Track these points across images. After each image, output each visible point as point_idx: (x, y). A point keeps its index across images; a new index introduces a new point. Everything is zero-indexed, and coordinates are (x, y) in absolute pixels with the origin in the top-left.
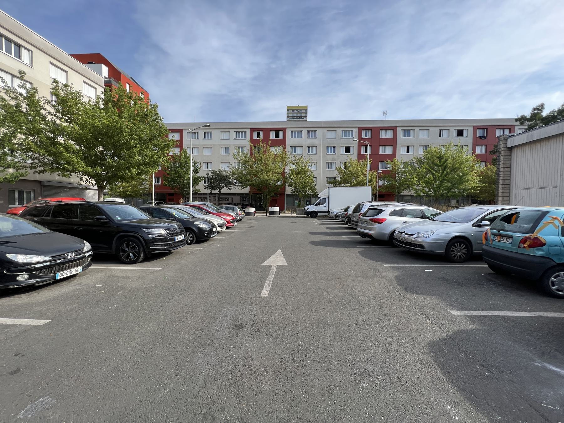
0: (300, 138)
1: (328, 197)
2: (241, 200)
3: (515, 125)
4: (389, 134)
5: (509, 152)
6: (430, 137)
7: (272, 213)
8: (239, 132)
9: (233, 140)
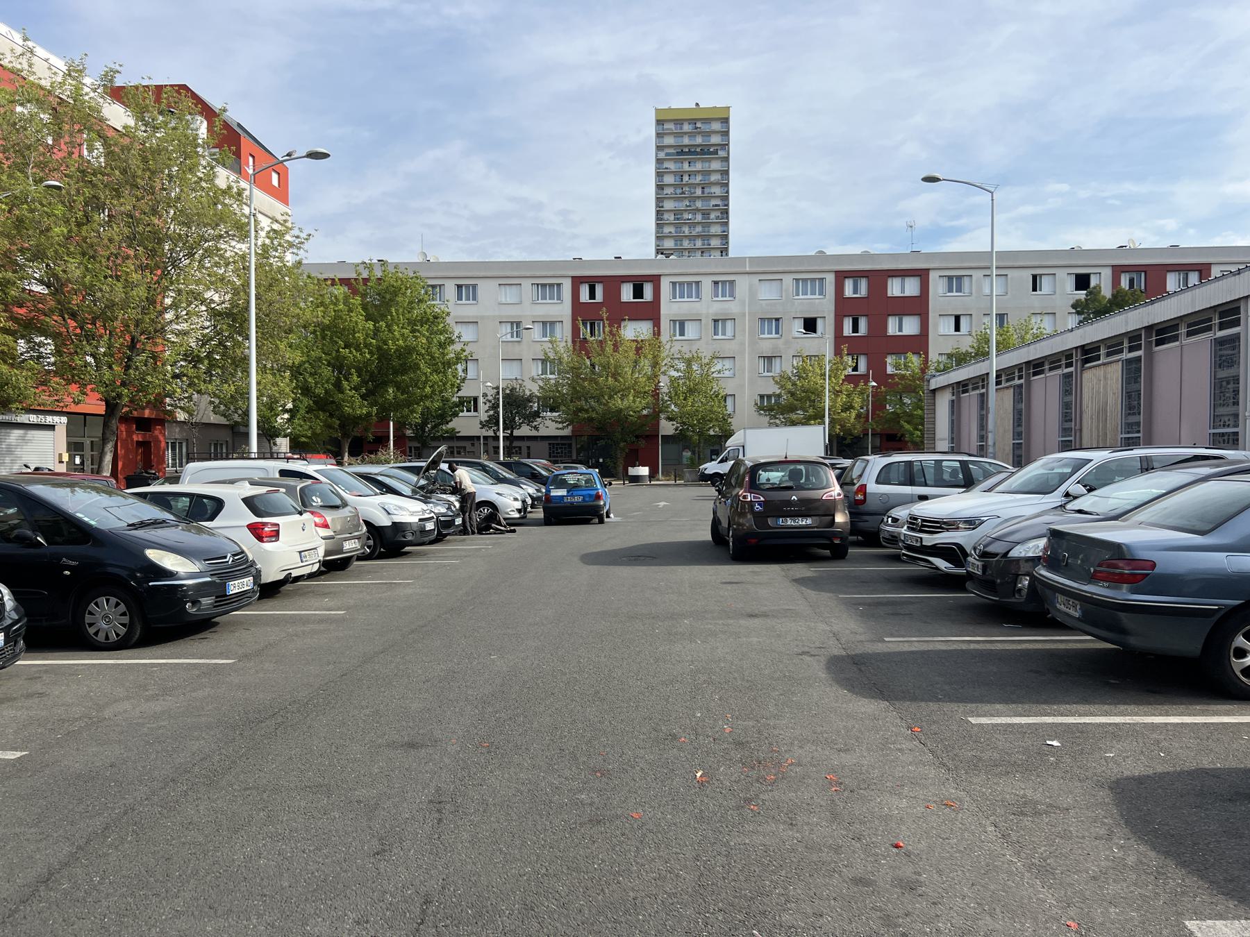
0: (693, 299)
1: (743, 447)
2: (550, 453)
3: (1211, 264)
4: (911, 288)
5: (932, 395)
6: (1009, 293)
7: (636, 479)
8: (544, 286)
9: (532, 308)
